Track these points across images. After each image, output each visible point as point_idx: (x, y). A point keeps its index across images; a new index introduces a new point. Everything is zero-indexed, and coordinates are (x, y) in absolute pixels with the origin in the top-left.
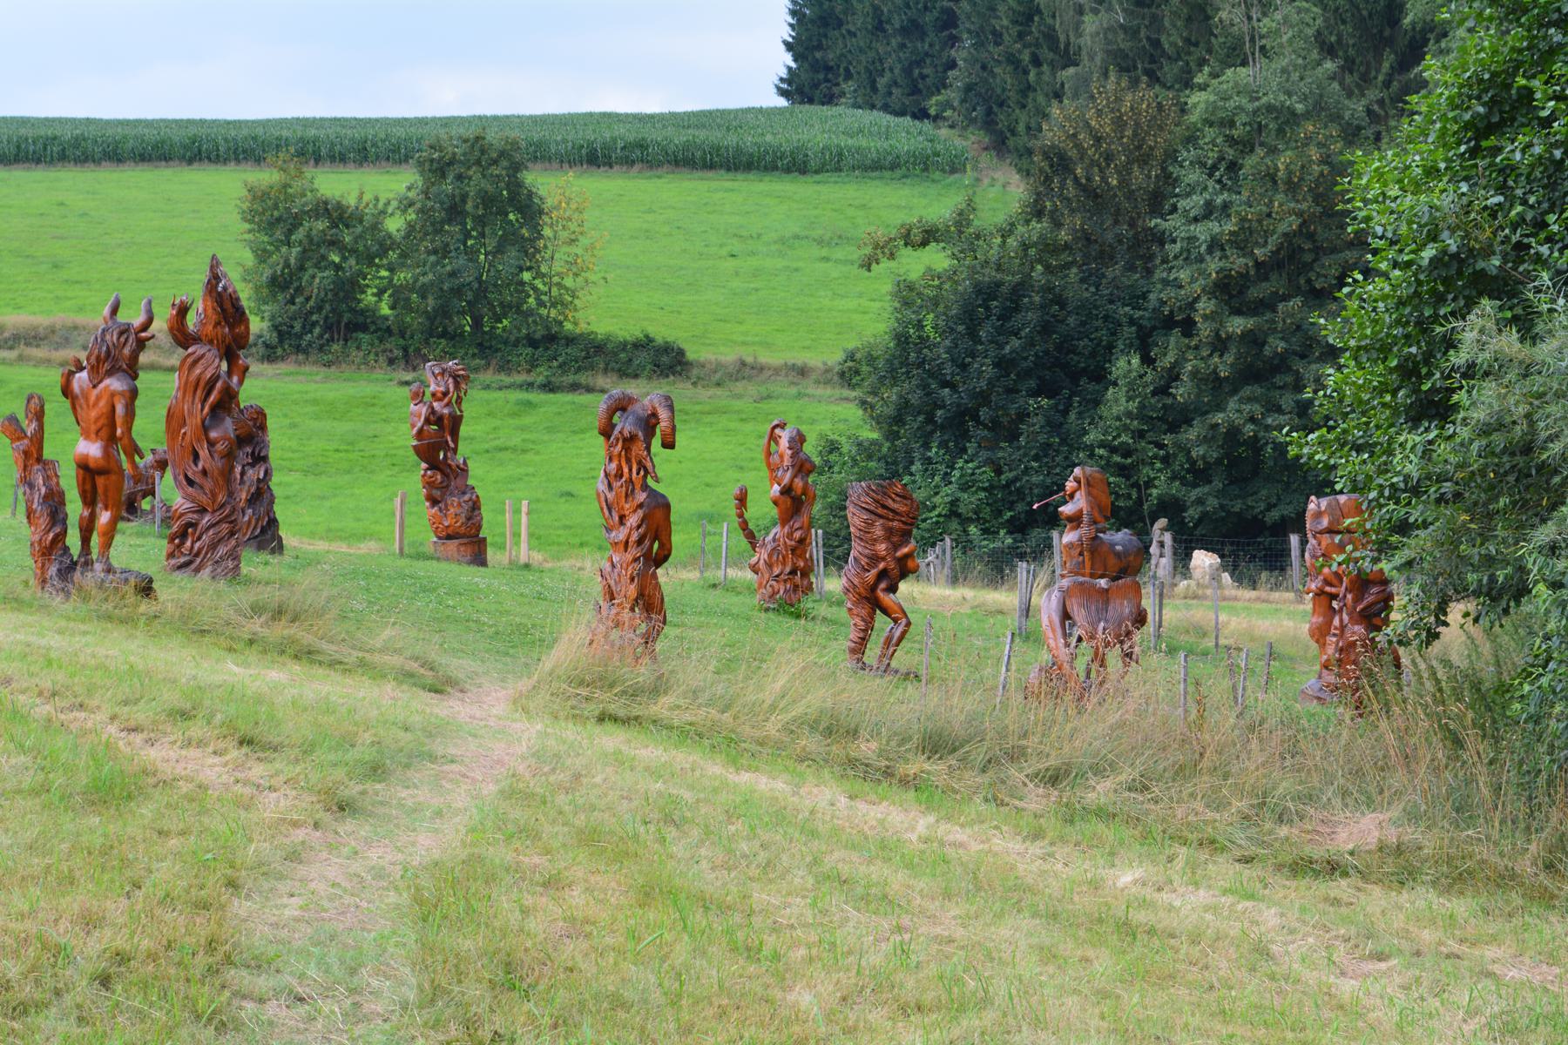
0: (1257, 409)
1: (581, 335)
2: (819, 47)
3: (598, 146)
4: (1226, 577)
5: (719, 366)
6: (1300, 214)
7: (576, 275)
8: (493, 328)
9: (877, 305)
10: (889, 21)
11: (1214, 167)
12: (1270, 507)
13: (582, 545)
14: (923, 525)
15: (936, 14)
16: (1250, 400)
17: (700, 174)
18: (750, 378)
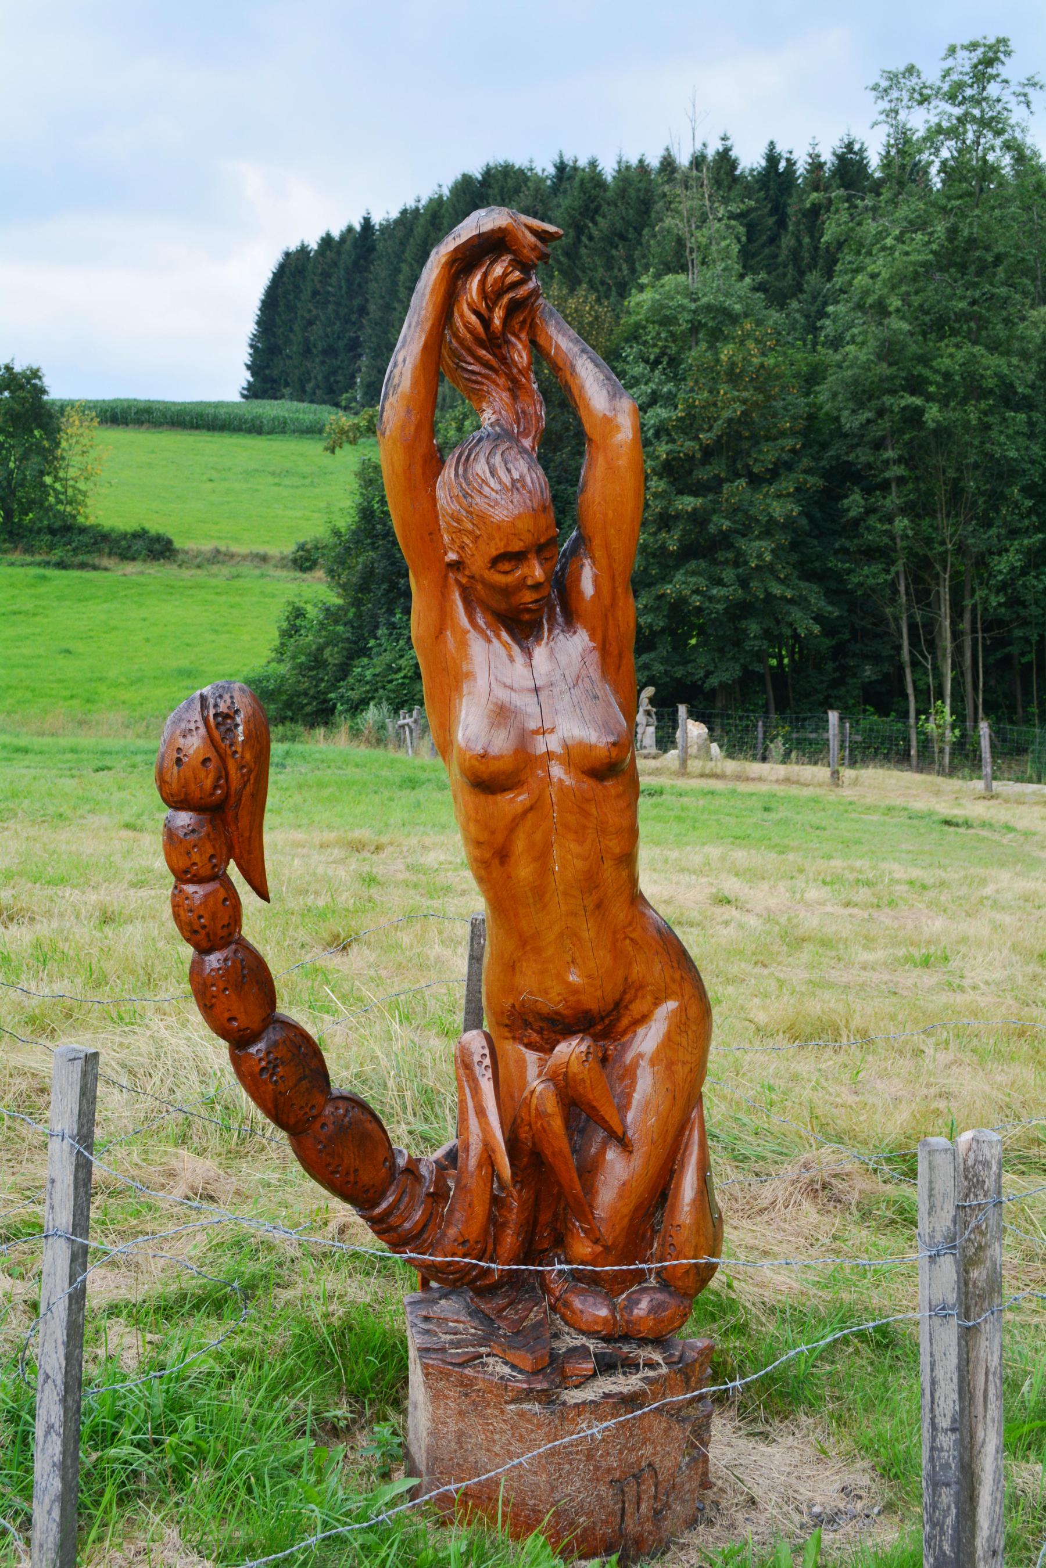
0: (702, 582)
1: (91, 526)
2: (268, 367)
3: (118, 411)
4: (714, 747)
5: (199, 554)
6: (744, 402)
7: (87, 479)
8: (21, 520)
9: (317, 515)
10: (315, 346)
11: (657, 362)
12: (708, 674)
13: (72, 697)
14: (389, 686)
15: (346, 341)
16: (693, 573)
17: (186, 432)
18: (223, 563)
